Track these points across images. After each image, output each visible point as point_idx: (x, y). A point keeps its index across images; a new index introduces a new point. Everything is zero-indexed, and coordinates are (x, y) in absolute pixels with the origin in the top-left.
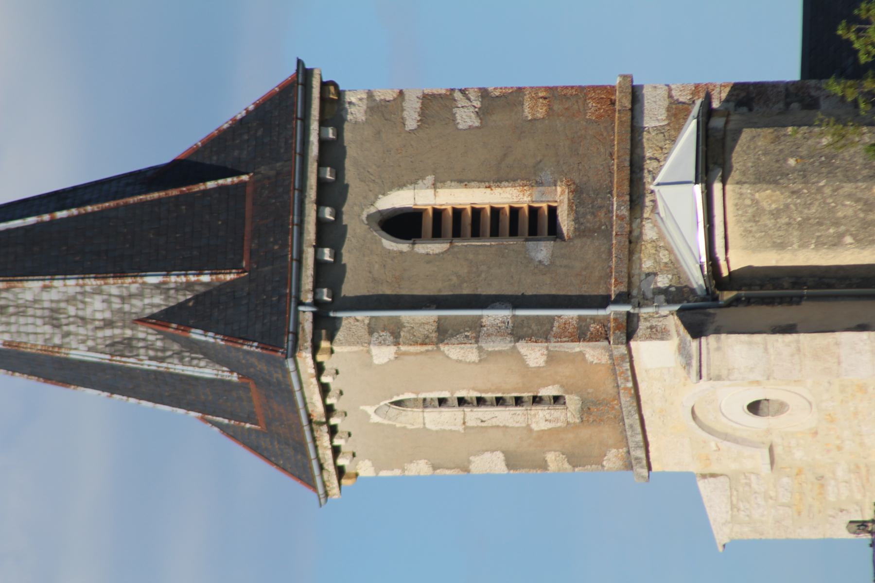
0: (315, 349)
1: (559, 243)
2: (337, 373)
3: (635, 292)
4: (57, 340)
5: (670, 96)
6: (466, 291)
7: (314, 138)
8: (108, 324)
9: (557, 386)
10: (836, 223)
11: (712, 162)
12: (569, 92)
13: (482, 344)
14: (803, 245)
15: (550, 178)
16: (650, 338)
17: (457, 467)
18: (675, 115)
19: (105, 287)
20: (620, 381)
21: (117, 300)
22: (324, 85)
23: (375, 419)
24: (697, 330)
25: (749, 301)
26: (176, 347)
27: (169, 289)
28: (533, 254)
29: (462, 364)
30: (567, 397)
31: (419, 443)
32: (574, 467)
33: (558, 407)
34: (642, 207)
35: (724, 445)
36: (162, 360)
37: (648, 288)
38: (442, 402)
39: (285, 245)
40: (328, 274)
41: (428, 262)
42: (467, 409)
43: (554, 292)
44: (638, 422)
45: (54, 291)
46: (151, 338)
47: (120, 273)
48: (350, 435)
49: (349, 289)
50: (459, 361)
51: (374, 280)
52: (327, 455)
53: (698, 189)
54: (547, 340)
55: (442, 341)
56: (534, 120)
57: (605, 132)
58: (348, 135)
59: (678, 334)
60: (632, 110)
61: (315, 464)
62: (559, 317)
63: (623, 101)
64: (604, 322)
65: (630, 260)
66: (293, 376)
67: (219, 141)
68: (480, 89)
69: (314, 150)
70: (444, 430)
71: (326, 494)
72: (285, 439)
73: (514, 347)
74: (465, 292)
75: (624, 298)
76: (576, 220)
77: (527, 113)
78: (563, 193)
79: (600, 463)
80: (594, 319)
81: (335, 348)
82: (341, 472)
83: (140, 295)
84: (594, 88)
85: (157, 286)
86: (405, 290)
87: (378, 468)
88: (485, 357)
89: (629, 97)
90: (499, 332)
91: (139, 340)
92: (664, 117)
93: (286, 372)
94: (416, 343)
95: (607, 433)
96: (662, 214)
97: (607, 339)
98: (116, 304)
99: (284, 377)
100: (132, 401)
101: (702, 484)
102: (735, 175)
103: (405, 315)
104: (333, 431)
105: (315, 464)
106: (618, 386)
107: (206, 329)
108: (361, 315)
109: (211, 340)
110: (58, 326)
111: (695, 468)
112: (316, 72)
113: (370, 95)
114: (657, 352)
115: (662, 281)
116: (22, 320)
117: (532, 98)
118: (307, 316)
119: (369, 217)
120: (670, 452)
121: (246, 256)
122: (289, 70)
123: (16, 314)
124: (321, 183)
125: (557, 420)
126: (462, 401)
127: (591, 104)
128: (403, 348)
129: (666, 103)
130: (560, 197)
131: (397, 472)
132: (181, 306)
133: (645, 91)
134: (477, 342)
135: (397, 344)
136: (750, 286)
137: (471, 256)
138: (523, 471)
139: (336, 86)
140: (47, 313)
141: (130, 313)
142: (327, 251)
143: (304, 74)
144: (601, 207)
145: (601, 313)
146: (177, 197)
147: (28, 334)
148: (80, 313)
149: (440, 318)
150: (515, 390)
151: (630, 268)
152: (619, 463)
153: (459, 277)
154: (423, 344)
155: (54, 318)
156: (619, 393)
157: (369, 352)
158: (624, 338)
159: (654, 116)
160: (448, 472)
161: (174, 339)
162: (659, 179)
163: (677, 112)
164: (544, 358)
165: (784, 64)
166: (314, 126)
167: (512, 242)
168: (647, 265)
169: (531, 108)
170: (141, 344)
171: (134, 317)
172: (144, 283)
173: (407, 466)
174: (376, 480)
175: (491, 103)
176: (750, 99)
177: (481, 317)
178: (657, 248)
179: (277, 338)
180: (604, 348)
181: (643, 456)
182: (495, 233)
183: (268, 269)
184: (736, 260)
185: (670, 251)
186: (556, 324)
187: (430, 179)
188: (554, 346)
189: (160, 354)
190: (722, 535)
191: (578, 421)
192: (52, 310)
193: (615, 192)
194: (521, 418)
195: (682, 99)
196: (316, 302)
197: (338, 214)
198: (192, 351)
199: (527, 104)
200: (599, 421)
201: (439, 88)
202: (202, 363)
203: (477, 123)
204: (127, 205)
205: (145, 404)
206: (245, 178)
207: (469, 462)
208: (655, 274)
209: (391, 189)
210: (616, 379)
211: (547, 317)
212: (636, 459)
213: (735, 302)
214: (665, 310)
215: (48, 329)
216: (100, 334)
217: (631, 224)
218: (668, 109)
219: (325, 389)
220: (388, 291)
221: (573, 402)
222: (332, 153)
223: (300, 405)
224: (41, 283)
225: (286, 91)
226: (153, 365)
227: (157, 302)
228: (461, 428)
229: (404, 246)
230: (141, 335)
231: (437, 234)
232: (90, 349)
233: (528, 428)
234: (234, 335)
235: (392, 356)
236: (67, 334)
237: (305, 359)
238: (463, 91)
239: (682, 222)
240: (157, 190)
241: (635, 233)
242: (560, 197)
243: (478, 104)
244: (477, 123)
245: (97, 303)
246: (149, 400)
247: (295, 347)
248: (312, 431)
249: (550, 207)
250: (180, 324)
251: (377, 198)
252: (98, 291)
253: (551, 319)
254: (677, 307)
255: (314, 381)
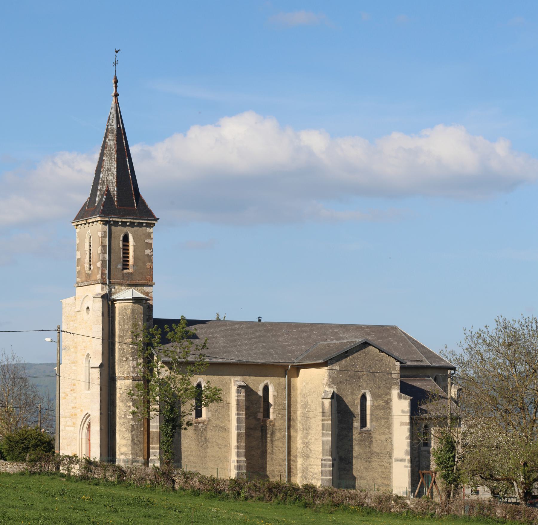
0: (101, 221)
7: (143, 221)
8: (107, 180)
10: (124, 325)
11: (136, 300)
14: (119, 318)
22: (154, 224)
24: (103, 297)
25: (109, 307)
29: (97, 250)
31: (83, 241)
35: (81, 302)
37: (112, 287)
38: (90, 246)
40: (116, 224)
47: (117, 182)
49: (113, 228)
52: (80, 223)
53: (131, 298)
57: (143, 279)
63: (150, 283)
64: (105, 278)
67: (143, 203)
69: (141, 221)
72: (84, 214)
75: (110, 282)
77: (148, 264)
82: (77, 225)
83: (113, 186)
87: (78, 233)
88: (99, 255)
90: (104, 258)
95: (84, 279)
98: (111, 182)
101: (73, 297)
102: (134, 305)
103: (107, 238)
104: (85, 224)
111: (77, 296)
113: (152, 233)
114: (98, 289)
115: (113, 290)
120: (80, 291)
122: (157, 217)
124: (135, 223)
126: (90, 250)
130: (131, 270)
132: (110, 194)
136: (112, 307)
143: (156, 220)
155: (109, 169)
159: (146, 289)
161: (104, 193)
163: (147, 294)
165: (157, 314)
166: (146, 221)
167: (122, 260)
168: (117, 287)
175: (150, 257)
176: (149, 308)
179: (103, 213)
182: (124, 257)
184: (117, 305)
188: (101, 268)
190: (63, 301)
196: (110, 221)
197: (128, 226)
213: (109, 305)
214: (107, 290)
219: (93, 222)
221: (90, 272)
222: (140, 225)
225: (153, 216)
227: (111, 189)
229: (121, 239)
231: (124, 245)
234: (104, 205)
237: (99, 219)
239: (125, 294)
242: (131, 270)
245: (112, 178)
247: (101, 217)
252: (114, 178)
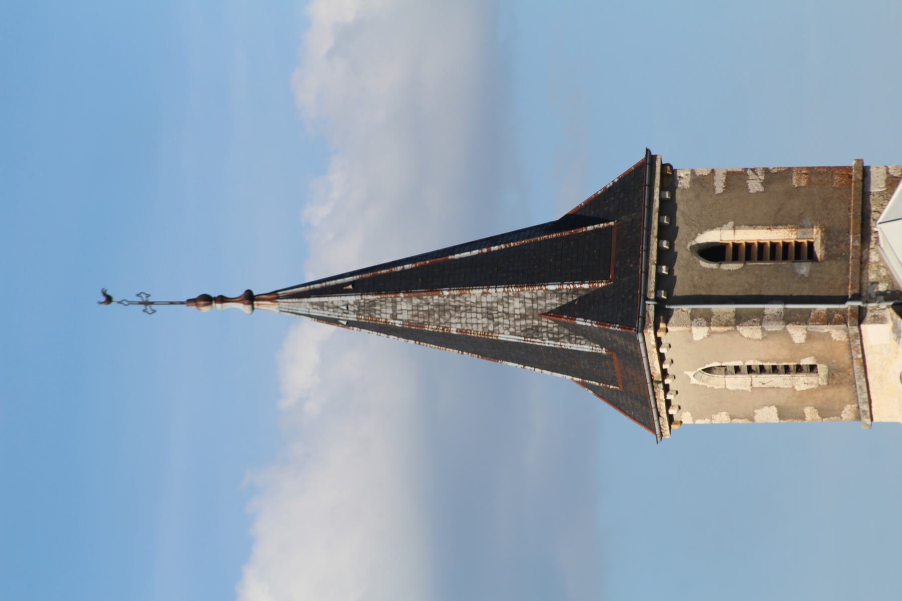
0: (656, 328)
1: (815, 263)
2: (670, 346)
3: (864, 294)
4: (491, 328)
5: (888, 173)
6: (754, 292)
7: (656, 198)
8: (524, 317)
9: (812, 358)
12: (822, 170)
13: (765, 326)
15: (809, 223)
16: (874, 322)
17: (746, 417)
18: (891, 184)
19: (522, 293)
20: (854, 353)
21: (530, 301)
22: (663, 166)
23: (694, 381)
26: (566, 331)
27: (562, 294)
28: (798, 270)
29: (751, 342)
30: (819, 366)
31: (722, 399)
32: (823, 418)
33: (813, 374)
34: (869, 241)
36: (557, 340)
38: (737, 369)
39: (637, 264)
40: (665, 282)
41: (729, 275)
42: (753, 376)
43: (811, 294)
44: (865, 384)
45: (489, 296)
46: (551, 326)
47: (532, 284)
48: (677, 392)
49: (678, 291)
50: (749, 339)
51: (695, 286)
52: (662, 405)
54: (807, 324)
55: (738, 324)
56: (799, 187)
58: (678, 197)
59: (892, 319)
60: (863, 181)
61: (654, 411)
62: (815, 309)
63: (857, 175)
64: (843, 313)
65: (861, 274)
66: (642, 345)
67: (595, 202)
68: (764, 169)
69: (656, 205)
70: (738, 390)
71: (662, 435)
73: (785, 329)
74: (754, 293)
75: (856, 297)
76: (826, 249)
77: (795, 183)
78: (817, 233)
79: (839, 415)
80: (837, 311)
81: (669, 328)
82: (671, 418)
83: (544, 298)
84: (838, 168)
85: (555, 292)
86: (714, 293)
87: (695, 418)
88: (767, 335)
89: (861, 173)
90: (776, 318)
91: (543, 327)
92: (884, 185)
93: (638, 343)
94: (721, 325)
95: (844, 392)
96: (882, 246)
97: (846, 323)
98: (529, 304)
99: (636, 348)
100: (537, 370)
103: (715, 308)
104: (666, 388)
105: (654, 411)
106: (852, 358)
107: (586, 318)
108: (687, 308)
109: (589, 325)
110: (493, 319)
112: (658, 157)
113: (693, 172)
115: (882, 287)
116: (469, 315)
117: (798, 174)
118: (651, 307)
119: (691, 247)
121: (612, 271)
123: (466, 311)
124: (661, 225)
125: (812, 383)
126: (750, 370)
127: (836, 177)
128: (713, 329)
129: (885, 177)
130: (815, 236)
131: (707, 421)
133: (871, 170)
134: (761, 324)
135: (709, 325)
137: (757, 272)
138: (789, 421)
139: (671, 167)
140: (484, 310)
141: (537, 309)
142: (664, 267)
143: (650, 159)
144: (842, 242)
145: (842, 306)
146: (568, 236)
147: (472, 324)
148: (506, 310)
149: (737, 310)
150: (785, 360)
151: (861, 279)
152: (852, 416)
153: (749, 284)
154: (726, 325)
155: (489, 313)
156: (852, 363)
157: (690, 331)
158: (857, 322)
160: (740, 421)
161: (565, 325)
162: (880, 220)
164: (804, 337)
166: (657, 190)
168: (872, 277)
169: (797, 180)
170: (544, 330)
171: (540, 312)
172: (547, 290)
173: (714, 416)
174: (694, 426)
175: (770, 177)
177: (763, 309)
178: (878, 267)
179: (632, 321)
180: (844, 329)
181: (868, 409)
182: (773, 258)
183: (625, 279)
185: (887, 269)
186: (812, 314)
187: (731, 224)
188: (812, 328)
189: (556, 336)
191: (825, 384)
192: (487, 308)
193: (851, 231)
194: (788, 382)
195: (895, 175)
196: (657, 299)
197: (671, 245)
198: (576, 334)
199: (795, 178)
200: (839, 384)
201: (738, 168)
202: (583, 342)
203: (762, 189)
204: (536, 242)
205: (545, 372)
206: (612, 223)
207: (754, 414)
208: (877, 283)
209: (705, 230)
210: (851, 353)
211: (807, 309)
212: (864, 411)
214: (883, 305)
215: (485, 320)
216: (518, 324)
217: (862, 251)
218: (887, 181)
219: (662, 358)
220: (703, 293)
222: (668, 207)
223: (646, 368)
224: (481, 291)
226: (551, 344)
228: (749, 388)
229: (714, 266)
230: (544, 324)
231: (735, 259)
232: (511, 334)
233: (793, 389)
235: (706, 335)
236: (498, 324)
237: (650, 334)
238: (753, 170)
240: (556, 232)
241: (865, 258)
242: (815, 236)
243: (762, 178)
244: (762, 189)
245: (517, 303)
246: (548, 370)
247: (644, 327)
248: (653, 387)
249: (809, 242)
250: (569, 316)
251: (696, 235)
253: (809, 311)
254: (891, 303)
255: (655, 350)
